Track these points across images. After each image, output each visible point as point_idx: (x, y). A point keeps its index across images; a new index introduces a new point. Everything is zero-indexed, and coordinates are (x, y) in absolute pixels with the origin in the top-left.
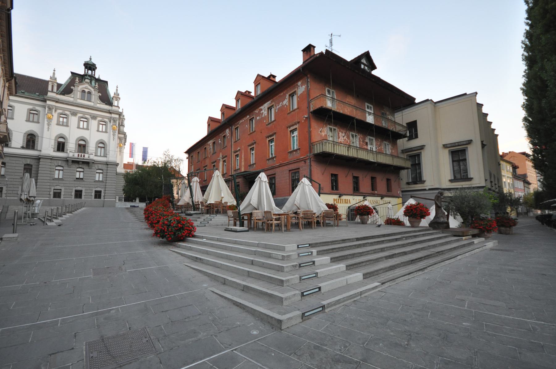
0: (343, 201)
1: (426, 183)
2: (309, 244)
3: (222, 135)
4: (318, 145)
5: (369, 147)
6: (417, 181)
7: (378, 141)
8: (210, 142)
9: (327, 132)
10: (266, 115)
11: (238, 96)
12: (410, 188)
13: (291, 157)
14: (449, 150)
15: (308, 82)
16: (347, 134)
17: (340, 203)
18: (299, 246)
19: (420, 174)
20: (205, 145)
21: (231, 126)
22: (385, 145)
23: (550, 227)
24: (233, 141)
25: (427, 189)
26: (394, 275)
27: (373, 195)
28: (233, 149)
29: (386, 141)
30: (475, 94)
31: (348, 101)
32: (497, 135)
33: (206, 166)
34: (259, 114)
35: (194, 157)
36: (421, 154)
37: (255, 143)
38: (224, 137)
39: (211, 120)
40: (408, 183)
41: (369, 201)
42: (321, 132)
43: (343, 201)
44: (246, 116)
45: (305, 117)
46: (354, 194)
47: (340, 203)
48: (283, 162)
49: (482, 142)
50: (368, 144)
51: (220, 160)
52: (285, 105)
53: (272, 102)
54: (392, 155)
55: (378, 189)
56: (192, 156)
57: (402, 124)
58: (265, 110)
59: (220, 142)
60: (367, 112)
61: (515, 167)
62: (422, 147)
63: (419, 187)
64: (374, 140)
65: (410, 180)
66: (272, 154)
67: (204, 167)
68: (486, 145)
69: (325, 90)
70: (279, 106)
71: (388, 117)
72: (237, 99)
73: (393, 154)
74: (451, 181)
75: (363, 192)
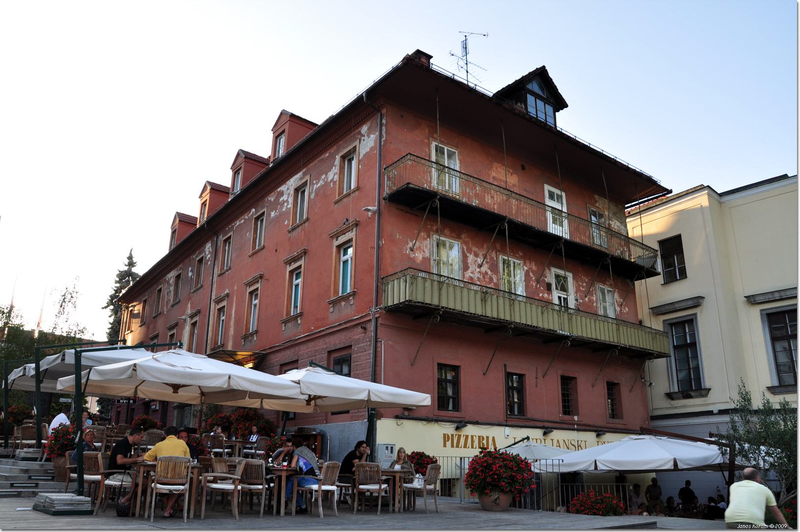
0: (473, 441)
3: (197, 256)
4: (396, 281)
6: (691, 389)
7: (583, 281)
11: (238, 162)
12: (676, 408)
13: (335, 316)
14: (761, 310)
16: (492, 259)
17: (465, 446)
19: (697, 369)
21: (217, 234)
24: (217, 271)
25: (715, 411)
29: (604, 283)
31: (494, 178)
34: (277, 204)
36: (696, 318)
38: (201, 261)
39: (183, 220)
40: (670, 396)
41: (555, 442)
42: (412, 250)
43: (473, 441)
44: (249, 209)
46: (509, 423)
47: (465, 446)
48: (317, 328)
50: (554, 286)
51: (185, 320)
52: (332, 180)
53: (304, 174)
57: (641, 242)
58: (289, 194)
59: (190, 274)
60: (550, 209)
62: (697, 302)
63: (694, 404)
65: (673, 387)
66: (296, 307)
69: (429, 149)
70: (319, 185)
72: (236, 169)
73: (625, 318)
74: (772, 389)
75: (536, 417)
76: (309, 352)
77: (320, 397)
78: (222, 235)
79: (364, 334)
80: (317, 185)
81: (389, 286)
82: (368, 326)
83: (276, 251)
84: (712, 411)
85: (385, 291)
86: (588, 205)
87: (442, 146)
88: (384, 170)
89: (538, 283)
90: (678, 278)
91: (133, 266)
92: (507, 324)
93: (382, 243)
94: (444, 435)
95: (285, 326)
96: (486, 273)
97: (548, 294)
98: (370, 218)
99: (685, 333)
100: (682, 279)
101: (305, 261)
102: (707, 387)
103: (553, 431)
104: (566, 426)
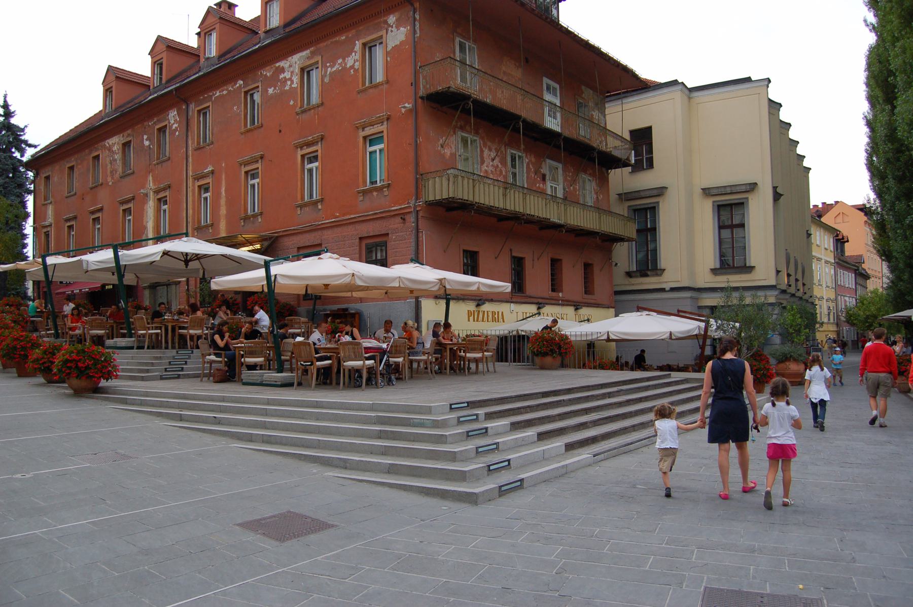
1: (666, 274)
2: (468, 403)
4: (437, 179)
5: (548, 187)
6: (648, 269)
8: (115, 142)
9: (457, 149)
10: (295, 85)
12: (633, 285)
15: (415, 19)
18: (453, 406)
19: (655, 251)
20: (97, 150)
21: (186, 101)
22: (584, 182)
23: (290, 304)
25: (667, 289)
26: (609, 445)
27: (555, 302)
28: (190, 168)
30: (766, 83)
32: (808, 169)
33: (100, 210)
34: (274, 80)
35: (55, 179)
36: (658, 205)
37: (262, 157)
38: (162, 130)
40: (629, 274)
42: (442, 146)
45: (405, 107)
46: (514, 300)
47: (483, 321)
48: (344, 215)
49: (775, 188)
51: (146, 195)
52: (352, 67)
53: (313, 53)
54: (598, 209)
55: (565, 287)
56: (47, 178)
57: (621, 135)
58: (292, 72)
59: (147, 143)
61: (840, 241)
62: (661, 191)
63: (650, 282)
64: (560, 171)
67: (93, 213)
68: (782, 195)
69: (454, 45)
70: (334, 69)
71: (592, 115)
74: (714, 271)
76: (335, 237)
77: (154, 261)
78: (193, 104)
79: (402, 225)
80: (331, 69)
81: (430, 182)
82: (407, 217)
83: (280, 131)
84: (665, 289)
85: (425, 187)
86: (576, 96)
87: (465, 42)
88: (420, 68)
89: (536, 174)
90: (645, 167)
91: (13, 117)
92: (520, 216)
93: (420, 141)
94: (468, 311)
95: (301, 210)
96: (497, 166)
97: (543, 185)
98: (403, 114)
99: (647, 218)
100: (649, 169)
101: (321, 146)
102: (663, 267)
103: (545, 306)
104: (554, 302)
